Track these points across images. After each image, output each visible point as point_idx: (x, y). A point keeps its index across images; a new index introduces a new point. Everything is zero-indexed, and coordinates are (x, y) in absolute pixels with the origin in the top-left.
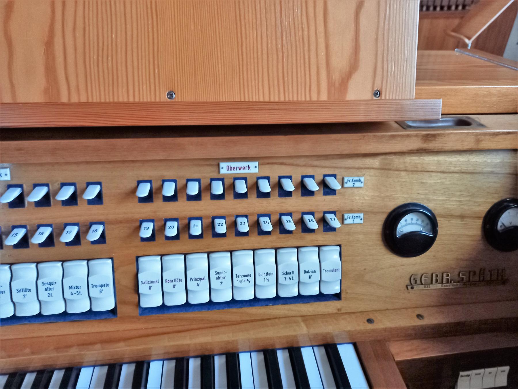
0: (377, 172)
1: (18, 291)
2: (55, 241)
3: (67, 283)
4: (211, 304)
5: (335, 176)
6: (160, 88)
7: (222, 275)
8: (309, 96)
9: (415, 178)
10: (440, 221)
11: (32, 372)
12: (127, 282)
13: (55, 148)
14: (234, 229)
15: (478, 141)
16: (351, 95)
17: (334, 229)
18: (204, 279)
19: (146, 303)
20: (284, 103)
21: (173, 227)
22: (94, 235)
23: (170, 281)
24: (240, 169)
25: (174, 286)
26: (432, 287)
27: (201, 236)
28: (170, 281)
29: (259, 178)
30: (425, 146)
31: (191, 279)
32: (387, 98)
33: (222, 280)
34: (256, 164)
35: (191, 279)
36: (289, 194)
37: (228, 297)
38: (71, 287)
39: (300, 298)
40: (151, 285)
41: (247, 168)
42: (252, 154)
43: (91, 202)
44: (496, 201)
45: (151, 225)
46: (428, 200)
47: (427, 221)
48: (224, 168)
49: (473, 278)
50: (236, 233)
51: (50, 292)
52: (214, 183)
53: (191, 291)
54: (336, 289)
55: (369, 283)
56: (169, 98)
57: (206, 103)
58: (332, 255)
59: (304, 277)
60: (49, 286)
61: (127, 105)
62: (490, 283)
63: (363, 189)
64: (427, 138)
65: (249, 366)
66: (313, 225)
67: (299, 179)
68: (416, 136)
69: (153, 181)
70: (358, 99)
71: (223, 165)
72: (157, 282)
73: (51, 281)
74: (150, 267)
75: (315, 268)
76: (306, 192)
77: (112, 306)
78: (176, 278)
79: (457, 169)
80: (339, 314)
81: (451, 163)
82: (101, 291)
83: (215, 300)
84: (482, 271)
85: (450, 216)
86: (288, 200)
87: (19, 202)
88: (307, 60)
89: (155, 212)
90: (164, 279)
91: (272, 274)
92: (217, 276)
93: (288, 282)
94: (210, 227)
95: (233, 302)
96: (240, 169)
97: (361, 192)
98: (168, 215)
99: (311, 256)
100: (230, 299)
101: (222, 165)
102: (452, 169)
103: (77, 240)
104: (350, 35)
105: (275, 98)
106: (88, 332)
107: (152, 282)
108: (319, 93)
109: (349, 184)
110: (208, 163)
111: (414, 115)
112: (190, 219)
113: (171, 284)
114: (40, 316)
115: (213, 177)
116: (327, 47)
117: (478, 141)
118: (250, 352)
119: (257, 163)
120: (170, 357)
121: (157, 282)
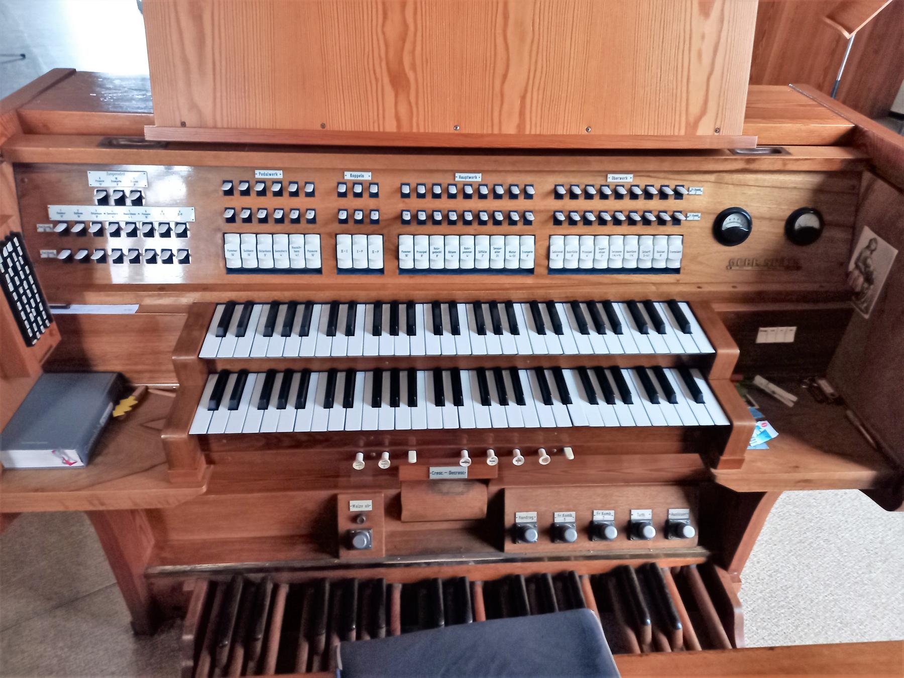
0: (712, 185)
1: (480, 252)
3: (656, 249)
5: (683, 186)
8: (674, 133)
9: (739, 190)
10: (755, 223)
11: (301, 303)
12: (543, 252)
15: (784, 164)
16: (700, 132)
20: (662, 136)
26: (745, 268)
29: (480, 185)
30: (747, 166)
34: (632, 176)
39: (474, 271)
42: (368, 167)
44: (796, 208)
46: (747, 206)
47: (744, 220)
48: (611, 178)
49: (775, 263)
54: (530, 265)
55: (701, 263)
57: (622, 136)
58: (677, 242)
59: (583, 256)
61: (636, 137)
62: (788, 268)
63: (702, 196)
64: (749, 161)
68: (742, 159)
70: (705, 134)
71: (610, 176)
75: (664, 249)
79: (769, 184)
80: (677, 283)
81: (765, 180)
84: (783, 259)
85: (762, 218)
86: (437, 201)
87: (230, 193)
90: (417, 251)
97: (701, 198)
98: (372, 208)
101: (457, 175)
102: (766, 184)
104: (702, 93)
105: (651, 133)
108: (679, 130)
109: (693, 192)
111: (743, 146)
112: (418, 211)
116: (687, 100)
117: (784, 164)
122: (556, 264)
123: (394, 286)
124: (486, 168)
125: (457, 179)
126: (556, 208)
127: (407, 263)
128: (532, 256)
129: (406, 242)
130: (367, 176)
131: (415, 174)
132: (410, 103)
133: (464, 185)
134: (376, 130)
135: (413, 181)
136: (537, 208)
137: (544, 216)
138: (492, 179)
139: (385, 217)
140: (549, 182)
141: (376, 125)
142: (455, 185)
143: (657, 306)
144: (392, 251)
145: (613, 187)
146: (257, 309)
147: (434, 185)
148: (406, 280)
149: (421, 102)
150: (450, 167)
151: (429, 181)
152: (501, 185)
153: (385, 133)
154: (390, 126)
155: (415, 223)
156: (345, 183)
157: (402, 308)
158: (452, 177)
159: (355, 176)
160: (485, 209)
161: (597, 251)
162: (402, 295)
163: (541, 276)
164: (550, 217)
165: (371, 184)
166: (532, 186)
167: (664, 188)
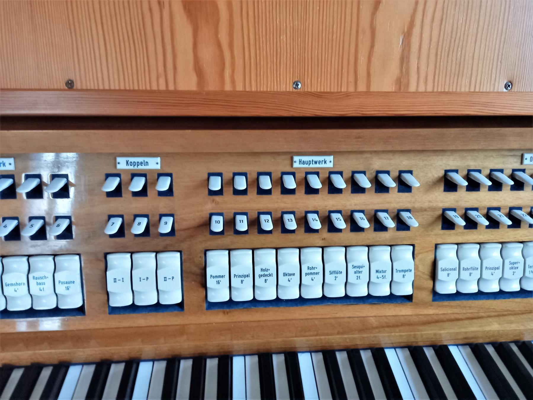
1: (331, 273)
2: (126, 232)
4: (324, 299)
6: (499, 79)
7: (515, 266)
11: (19, 367)
12: (427, 269)
13: (390, 137)
14: (256, 227)
17: (361, 229)
18: (248, 276)
19: (213, 297)
21: (218, 222)
22: (166, 227)
23: (467, 269)
24: (316, 163)
25: (470, 274)
27: (222, 233)
28: (467, 269)
31: (486, 268)
32: (259, 90)
33: (514, 270)
35: (486, 268)
36: (316, 191)
37: (295, 295)
38: (377, 271)
40: (449, 272)
41: (2, 165)
43: (136, 194)
45: (170, 220)
48: (298, 162)
50: (258, 230)
51: (358, 275)
52: (237, 178)
53: (234, 288)
54: (408, 290)
56: (295, 88)
59: (486, 274)
60: (358, 269)
65: (243, 369)
66: (316, 225)
67: (397, 174)
69: (173, 175)
72: (455, 269)
73: (360, 265)
74: (119, 263)
76: (357, 188)
77: (179, 300)
78: (472, 266)
82: (404, 276)
83: (259, 298)
86: (265, 198)
88: (292, 50)
89: (457, 201)
90: (231, 273)
91: (24, 284)
92: (511, 266)
93: (380, 280)
94: (255, 224)
95: (278, 301)
96: (316, 163)
98: (163, 211)
99: (382, 254)
100: (275, 297)
101: (296, 158)
103: (121, 233)
106: (116, 326)
107: (451, 270)
110: (512, 153)
112: (236, 214)
113: (468, 272)
114: (369, 296)
115: (515, 168)
118: (244, 356)
119: (332, 157)
120: (465, 343)
121: (455, 269)
122: (446, 286)
123: (198, 333)
124: (343, 148)
125: (296, 165)
126: (447, 205)
127: (218, 293)
128: (411, 276)
129: (217, 261)
130: (154, 164)
131: (231, 155)
132: (219, 45)
133: (307, 173)
134: (162, 87)
135: (228, 171)
136: (417, 205)
137: (428, 217)
138: (349, 164)
139: (185, 225)
140: (437, 166)
141: (162, 81)
142: (293, 174)
143: (454, 351)
144: (195, 276)
145: (300, 176)
146: (73, 373)
147: (260, 174)
148: (218, 318)
149: (237, 43)
150: (286, 148)
151: (252, 169)
152: (364, 173)
153: (176, 93)
154: (187, 82)
155: (232, 233)
156: (118, 175)
157: (212, 365)
158: (288, 162)
159: (134, 164)
160: (339, 208)
161: (507, 266)
162: (213, 344)
163: (424, 304)
164: (438, 218)
165: (160, 175)
166: (411, 172)
167: (498, 174)
